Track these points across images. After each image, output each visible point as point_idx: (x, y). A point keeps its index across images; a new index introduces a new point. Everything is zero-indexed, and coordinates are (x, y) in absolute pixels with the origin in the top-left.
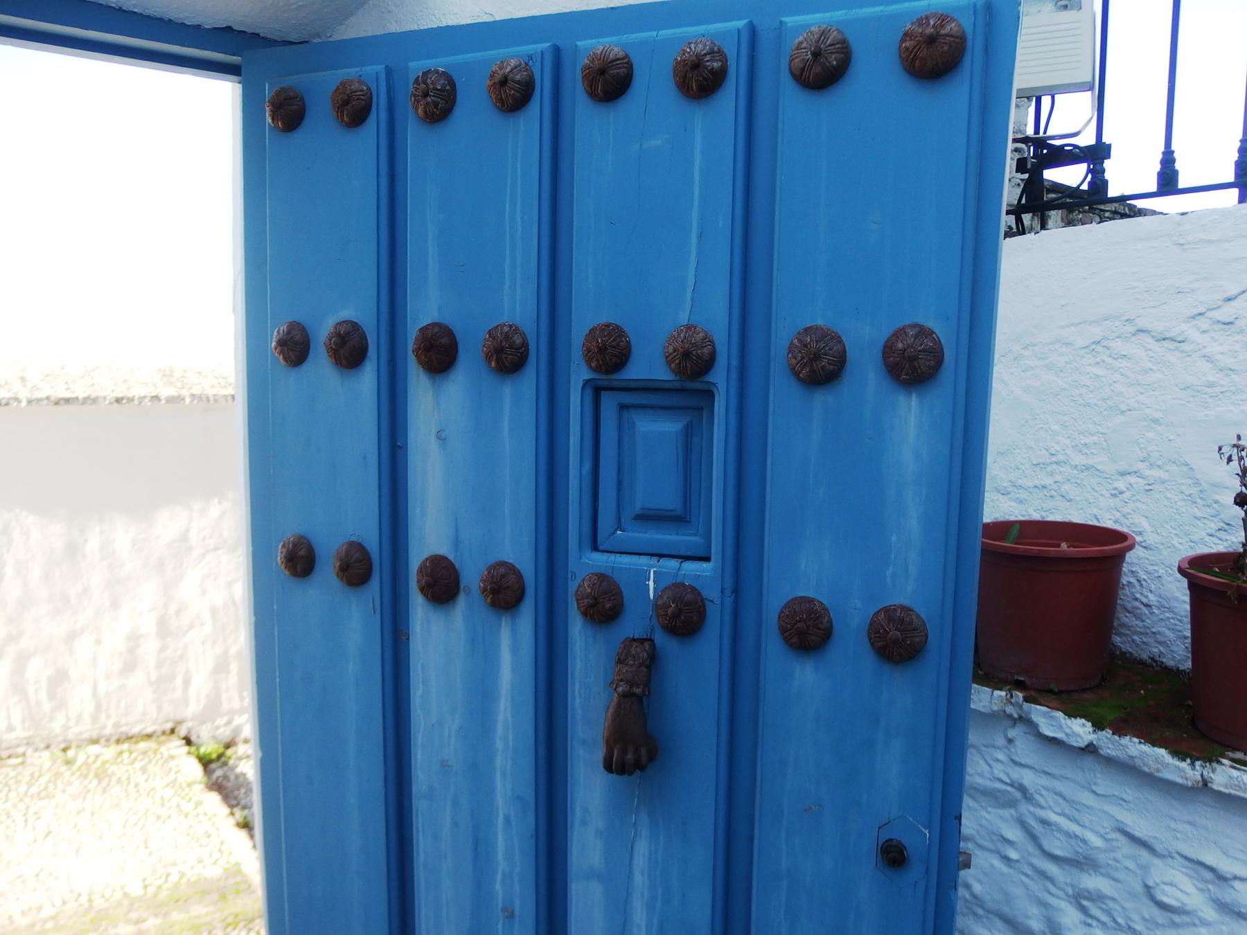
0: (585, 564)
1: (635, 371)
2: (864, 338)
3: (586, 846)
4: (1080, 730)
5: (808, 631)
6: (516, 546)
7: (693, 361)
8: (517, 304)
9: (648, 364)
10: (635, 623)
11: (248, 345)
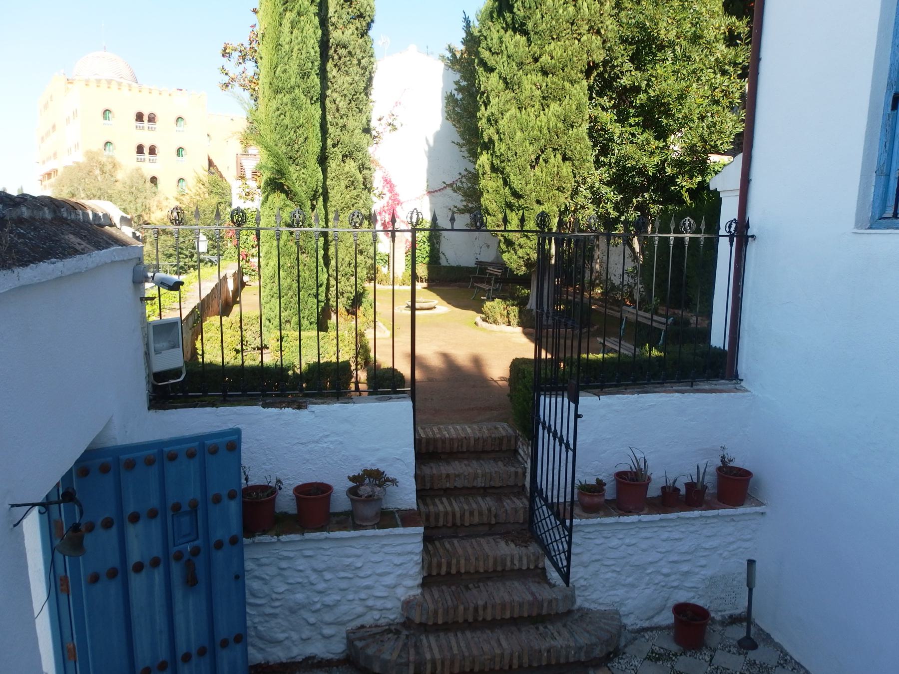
0: (173, 550)
1: (182, 510)
2: (224, 493)
3: (178, 606)
4: (293, 537)
5: (219, 545)
6: (157, 552)
7: (194, 506)
8: (154, 502)
9: (185, 507)
10: (186, 557)
11: (869, 111)
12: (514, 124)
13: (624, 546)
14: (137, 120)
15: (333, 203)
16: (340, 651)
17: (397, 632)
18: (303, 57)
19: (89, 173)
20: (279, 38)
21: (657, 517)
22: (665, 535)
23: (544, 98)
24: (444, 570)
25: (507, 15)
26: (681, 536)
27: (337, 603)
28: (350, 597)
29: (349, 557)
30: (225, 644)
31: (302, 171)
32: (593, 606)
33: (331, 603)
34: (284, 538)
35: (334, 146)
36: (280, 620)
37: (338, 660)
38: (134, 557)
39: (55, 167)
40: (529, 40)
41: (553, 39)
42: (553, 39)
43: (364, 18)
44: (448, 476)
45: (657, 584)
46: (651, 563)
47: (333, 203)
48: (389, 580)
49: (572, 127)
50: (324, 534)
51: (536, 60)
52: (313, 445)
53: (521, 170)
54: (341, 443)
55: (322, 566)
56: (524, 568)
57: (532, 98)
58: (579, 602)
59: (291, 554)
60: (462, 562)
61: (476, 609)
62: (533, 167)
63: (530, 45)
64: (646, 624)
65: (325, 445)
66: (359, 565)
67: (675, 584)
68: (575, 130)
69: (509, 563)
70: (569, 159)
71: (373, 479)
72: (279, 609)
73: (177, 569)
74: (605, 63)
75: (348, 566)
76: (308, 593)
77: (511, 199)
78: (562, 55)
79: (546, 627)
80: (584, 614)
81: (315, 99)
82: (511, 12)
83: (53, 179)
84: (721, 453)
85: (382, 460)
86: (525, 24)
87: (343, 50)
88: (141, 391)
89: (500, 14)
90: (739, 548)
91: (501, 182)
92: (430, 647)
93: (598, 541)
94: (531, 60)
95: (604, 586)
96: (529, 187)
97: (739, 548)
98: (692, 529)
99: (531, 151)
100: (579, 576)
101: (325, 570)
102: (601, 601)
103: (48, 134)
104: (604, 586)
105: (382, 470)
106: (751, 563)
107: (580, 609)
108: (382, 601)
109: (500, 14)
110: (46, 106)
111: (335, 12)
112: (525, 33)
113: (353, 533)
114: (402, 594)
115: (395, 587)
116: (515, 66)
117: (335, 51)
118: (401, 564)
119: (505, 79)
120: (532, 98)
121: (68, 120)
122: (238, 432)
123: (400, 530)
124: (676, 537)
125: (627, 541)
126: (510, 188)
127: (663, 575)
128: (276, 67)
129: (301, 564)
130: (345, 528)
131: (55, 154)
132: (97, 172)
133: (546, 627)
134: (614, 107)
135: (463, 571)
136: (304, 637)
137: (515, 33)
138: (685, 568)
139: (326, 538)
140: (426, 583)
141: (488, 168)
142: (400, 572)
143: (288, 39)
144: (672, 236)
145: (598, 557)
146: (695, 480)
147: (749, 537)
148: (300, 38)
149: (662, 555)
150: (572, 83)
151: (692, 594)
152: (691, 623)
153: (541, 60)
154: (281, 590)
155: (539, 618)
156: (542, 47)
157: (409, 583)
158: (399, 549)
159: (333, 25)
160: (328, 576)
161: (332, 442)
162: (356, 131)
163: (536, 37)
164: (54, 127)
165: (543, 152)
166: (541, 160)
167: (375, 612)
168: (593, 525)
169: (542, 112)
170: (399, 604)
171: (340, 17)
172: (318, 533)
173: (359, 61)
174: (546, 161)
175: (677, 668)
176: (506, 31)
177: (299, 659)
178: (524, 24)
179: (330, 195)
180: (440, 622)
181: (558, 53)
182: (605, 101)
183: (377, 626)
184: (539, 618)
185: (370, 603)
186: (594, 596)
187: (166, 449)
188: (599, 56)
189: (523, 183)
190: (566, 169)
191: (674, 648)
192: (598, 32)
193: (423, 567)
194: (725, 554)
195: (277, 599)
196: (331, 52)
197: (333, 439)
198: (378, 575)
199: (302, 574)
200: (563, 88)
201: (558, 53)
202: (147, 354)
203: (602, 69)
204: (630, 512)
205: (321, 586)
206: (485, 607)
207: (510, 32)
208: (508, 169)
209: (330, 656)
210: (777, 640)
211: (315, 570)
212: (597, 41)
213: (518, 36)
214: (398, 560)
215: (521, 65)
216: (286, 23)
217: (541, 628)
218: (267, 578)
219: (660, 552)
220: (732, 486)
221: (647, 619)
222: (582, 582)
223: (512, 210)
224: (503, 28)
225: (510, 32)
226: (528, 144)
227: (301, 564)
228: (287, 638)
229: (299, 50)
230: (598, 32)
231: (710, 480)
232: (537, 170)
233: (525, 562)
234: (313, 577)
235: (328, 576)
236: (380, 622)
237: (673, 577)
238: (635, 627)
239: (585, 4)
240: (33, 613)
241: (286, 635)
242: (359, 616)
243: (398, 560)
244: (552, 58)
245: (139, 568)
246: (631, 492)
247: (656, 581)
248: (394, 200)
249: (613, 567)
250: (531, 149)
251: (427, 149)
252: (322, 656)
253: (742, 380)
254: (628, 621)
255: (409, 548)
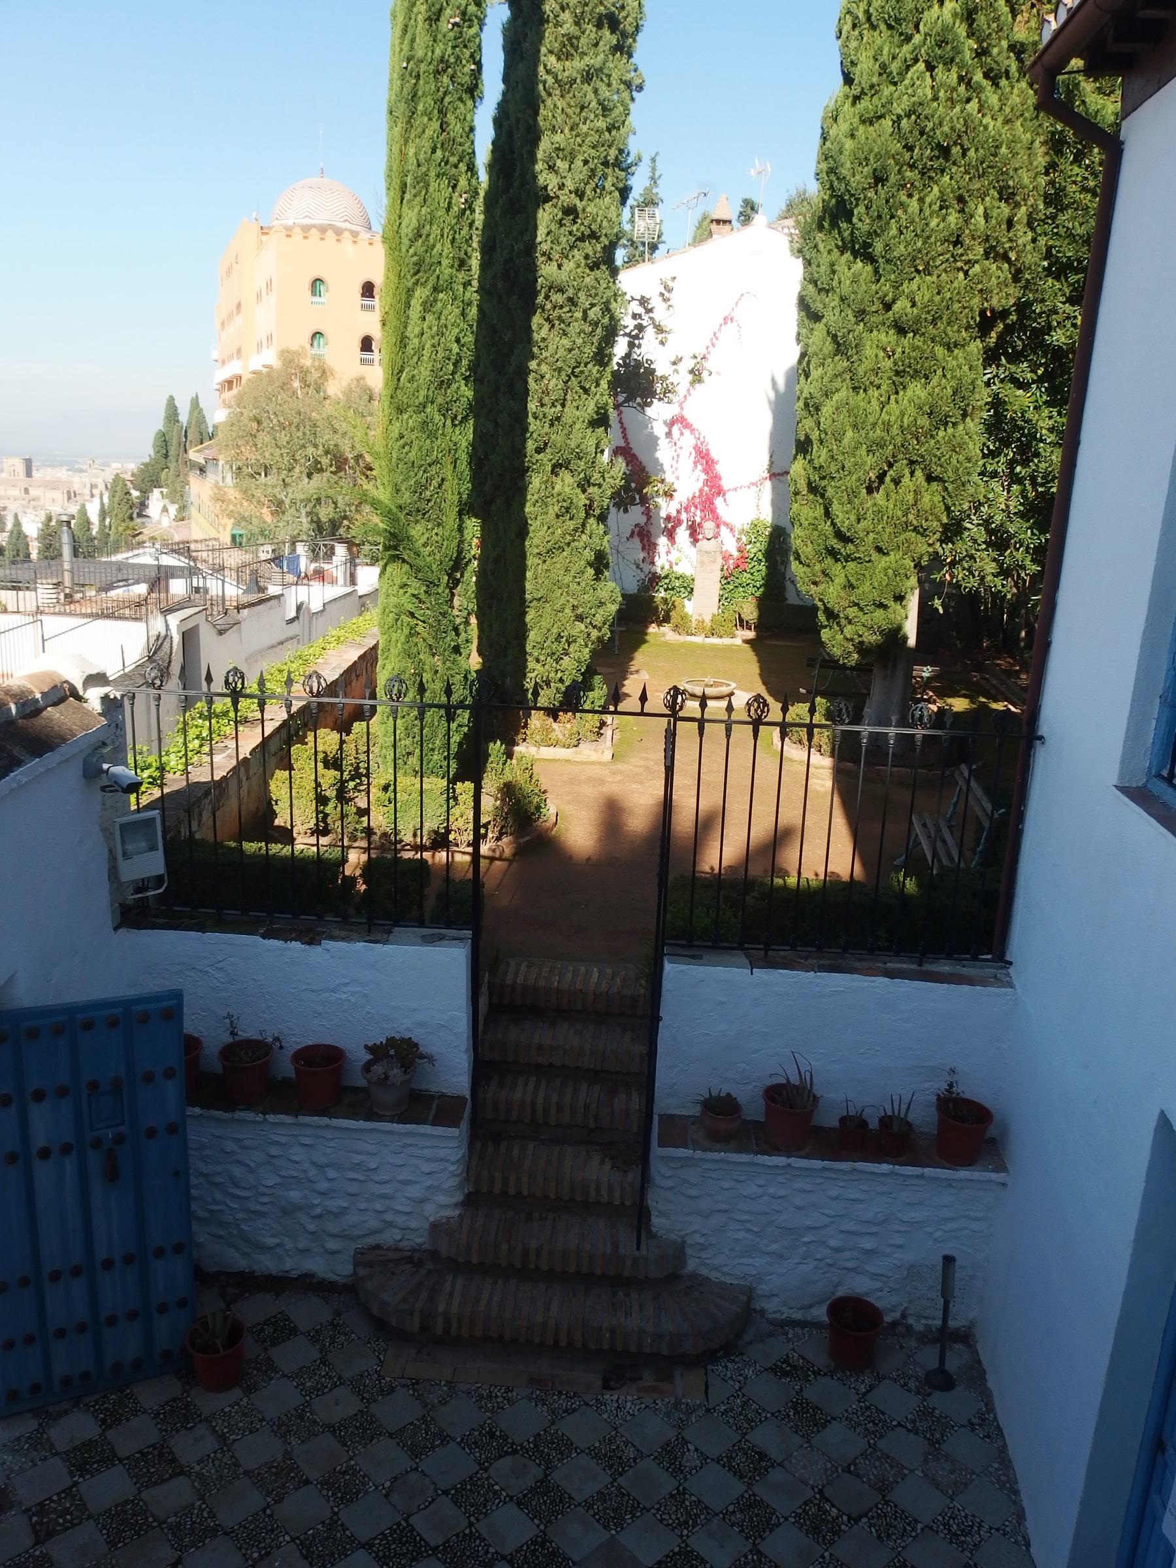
5: (151, 1133)
12: (843, 417)
13: (766, 1198)
14: (363, 295)
15: (535, 541)
16: (347, 1273)
17: (420, 1264)
18: (440, 355)
19: (284, 386)
20: (406, 327)
21: (818, 1164)
22: (834, 1192)
23: (897, 373)
24: (497, 1189)
25: (844, 225)
26: (862, 1197)
27: (343, 1212)
28: (362, 1206)
29: (360, 1153)
30: (160, 1253)
31: (435, 531)
32: (713, 1275)
33: (335, 1210)
34: (271, 1118)
35: (539, 451)
36: (269, 1221)
37: (345, 1285)
38: (40, 1140)
39: (239, 372)
40: (876, 271)
41: (918, 271)
42: (918, 271)
43: (597, 238)
44: (540, 1047)
45: (820, 1260)
46: (809, 1228)
47: (535, 541)
48: (414, 1192)
49: (946, 423)
50: (324, 1120)
51: (888, 307)
52: (327, 995)
53: (852, 494)
54: (365, 996)
55: (323, 1160)
56: (617, 1202)
57: (876, 371)
58: (691, 1265)
59: (284, 1140)
60: (525, 1180)
61: (526, 1253)
62: (870, 490)
63: (878, 281)
64: (798, 1316)
65: (343, 996)
66: (373, 1165)
67: (851, 1265)
68: (950, 430)
69: (593, 1193)
70: (938, 479)
71: (402, 1053)
72: (268, 1206)
73: (94, 1159)
74: (1023, 308)
75: (358, 1164)
76: (306, 1192)
77: (834, 543)
78: (931, 300)
79: (627, 1295)
80: (697, 1282)
81: (459, 418)
82: (850, 222)
83: (235, 391)
84: (949, 1079)
85: (421, 1025)
86: (870, 245)
87: (559, 295)
88: (100, 905)
89: (834, 225)
90: (963, 1228)
91: (820, 511)
92: (451, 1294)
93: (726, 1185)
94: (878, 306)
95: (732, 1250)
96: (863, 524)
97: (963, 1228)
98: (881, 1189)
99: (870, 464)
100: (692, 1229)
101: (327, 1166)
102: (726, 1269)
103: (230, 317)
104: (732, 1250)
105: (415, 1040)
106: (949, 1260)
107: (694, 1276)
108: (404, 1218)
109: (834, 225)
110: (229, 272)
111: (548, 233)
112: (870, 259)
113: (361, 1124)
114: (431, 1212)
115: (422, 1201)
116: (851, 317)
117: (547, 297)
118: (430, 1173)
119: (835, 337)
120: (876, 371)
121: (259, 296)
122: (178, 995)
123: (426, 1129)
124: (852, 1196)
125: (771, 1190)
126: (833, 524)
127: (831, 1248)
128: (401, 371)
129: (297, 1153)
130: (354, 1116)
131: (239, 351)
132: (296, 384)
133: (627, 1295)
134: (1040, 380)
135: (525, 1193)
136: (300, 1246)
137: (855, 258)
138: (867, 1244)
139: (327, 1126)
140: (471, 1201)
141: (803, 486)
142: (428, 1183)
143: (417, 330)
144: (892, 731)
145: (723, 1207)
146: (890, 1113)
147: (978, 1214)
148: (435, 329)
149: (829, 1220)
150: (949, 349)
151: (878, 1285)
152: (855, 1328)
153: (896, 307)
154: (270, 1183)
155: (617, 1281)
156: (897, 286)
157: (442, 1199)
158: (427, 1153)
159: (544, 254)
160: (332, 1173)
161: (353, 994)
162: (577, 426)
163: (888, 267)
164: (239, 306)
165: (890, 465)
166: (888, 479)
167: (396, 1231)
168: (716, 1161)
169: (893, 397)
170: (427, 1226)
171: (556, 241)
172: (316, 1118)
173: (585, 312)
174: (896, 482)
175: (807, 1394)
176: (842, 253)
177: (294, 1274)
178: (867, 245)
179: (531, 529)
180: (475, 1261)
181: (923, 296)
182: (1023, 370)
183: (397, 1249)
184: (617, 1281)
185: (389, 1217)
186: (717, 1261)
187: (79, 1016)
188: (1004, 297)
189: (853, 518)
190: (931, 497)
191: (821, 1360)
192: (1005, 257)
193: (467, 1179)
194: (938, 1234)
195: (264, 1194)
196: (540, 299)
197: (355, 989)
198: (400, 1182)
199: (297, 1166)
200: (934, 357)
201: (923, 296)
202: (113, 859)
203: (1014, 317)
204: (778, 1150)
205: (323, 1186)
206: (538, 1252)
207: (848, 255)
208: (830, 492)
209: (334, 1278)
210: (990, 1385)
211: (314, 1164)
212: (1003, 271)
213: (860, 264)
214: (426, 1167)
215: (861, 315)
216: (415, 312)
217: (621, 1294)
218: (252, 1165)
219: (827, 1216)
220: (964, 1132)
221: (801, 1309)
222: (697, 1238)
223: (837, 560)
224: (837, 247)
225: (848, 255)
226: (864, 453)
227: (297, 1153)
228: (278, 1245)
229: (433, 346)
230: (1005, 257)
231: (924, 1116)
232: (879, 497)
233: (617, 1194)
234: (313, 1172)
235: (332, 1173)
236: (402, 1245)
237: (847, 1254)
238: (778, 1316)
239: (981, 210)
240: (949, 697)
241: (277, 1241)
242: (373, 1233)
243: (426, 1167)
244: (914, 305)
245: (45, 1154)
246: (789, 1120)
247: (818, 1256)
248: (711, 488)
249: (748, 1225)
250: (870, 460)
251: (772, 395)
252: (322, 1275)
253: (1011, 963)
254: (770, 1306)
255: (442, 1153)
